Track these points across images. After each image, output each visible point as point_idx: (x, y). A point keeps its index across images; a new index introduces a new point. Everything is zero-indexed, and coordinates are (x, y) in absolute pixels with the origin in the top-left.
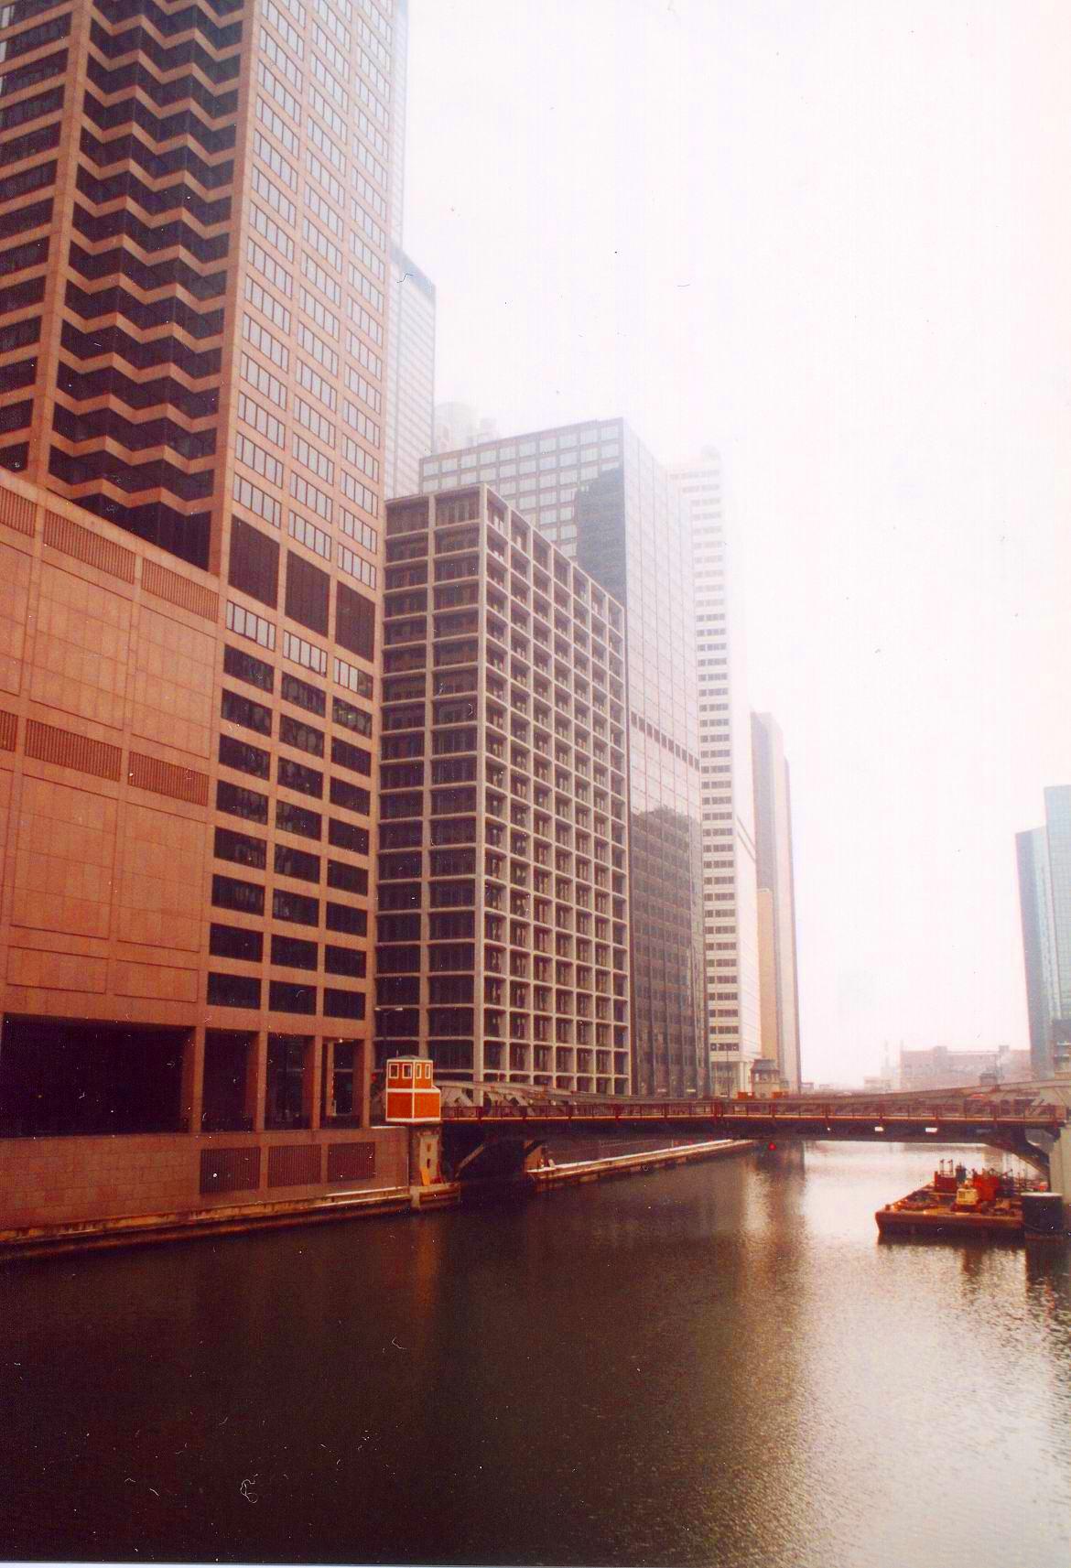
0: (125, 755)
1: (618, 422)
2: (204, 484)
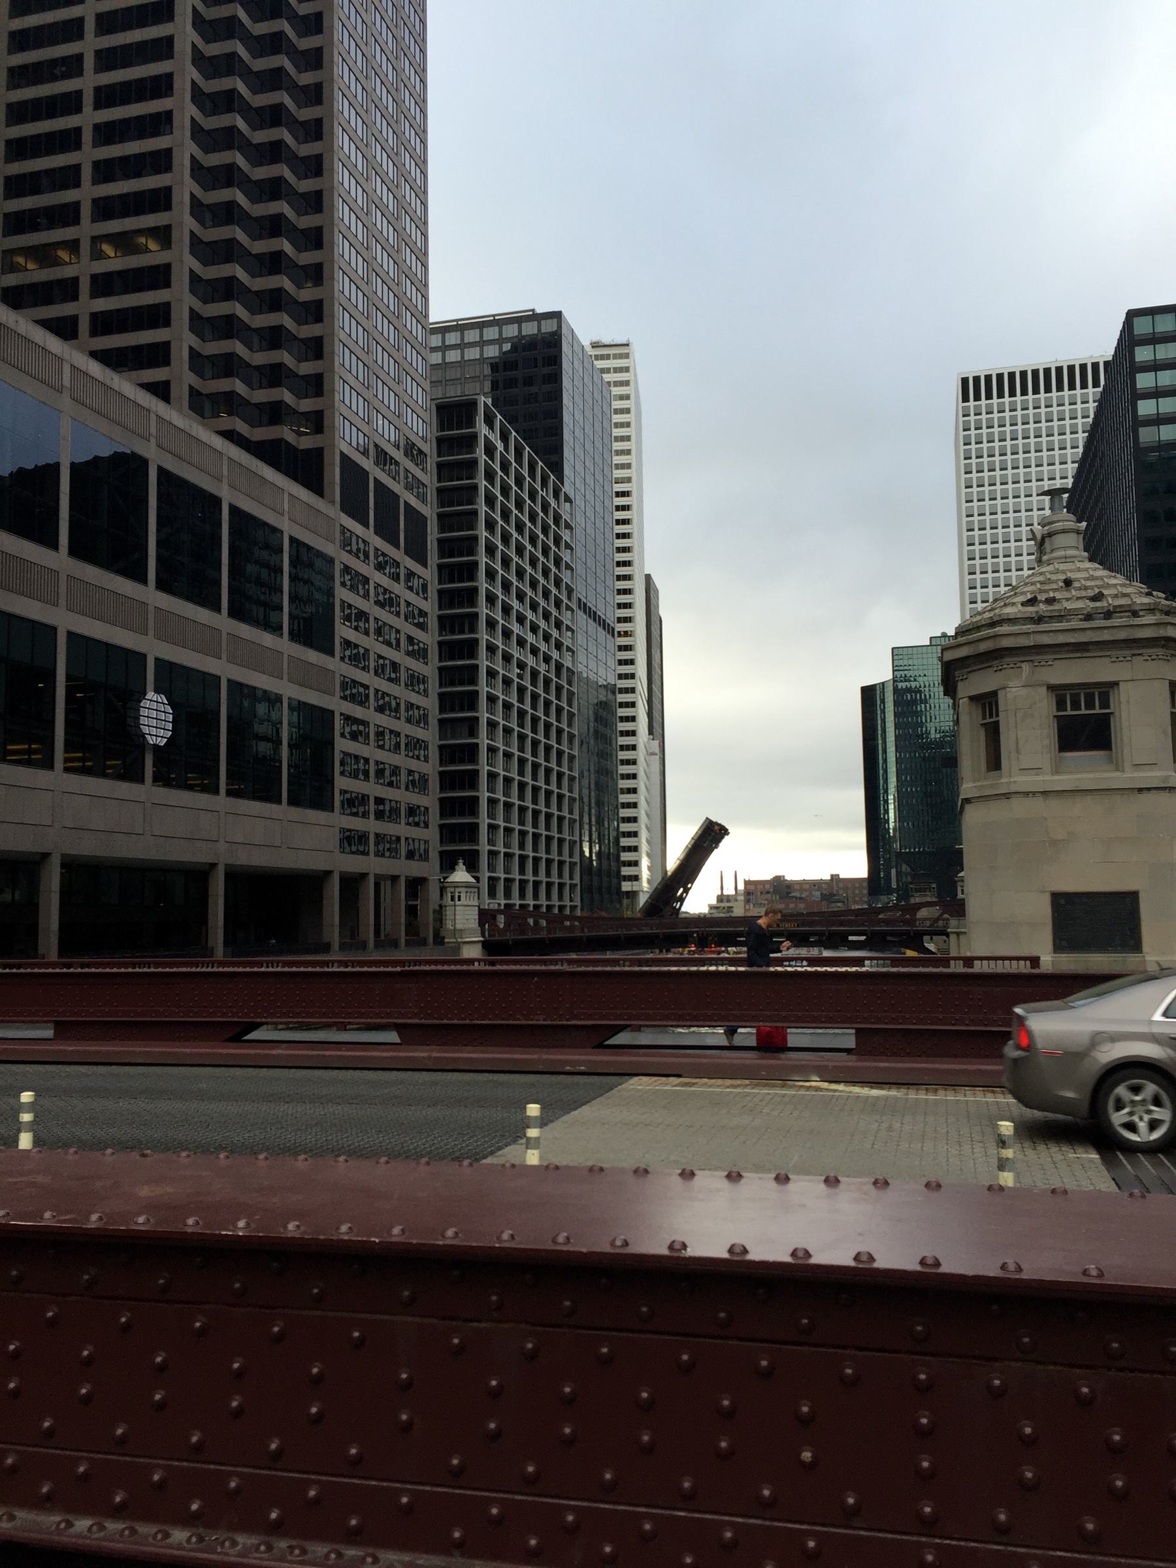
0: (151, 632)
1: (557, 316)
2: (318, 422)
